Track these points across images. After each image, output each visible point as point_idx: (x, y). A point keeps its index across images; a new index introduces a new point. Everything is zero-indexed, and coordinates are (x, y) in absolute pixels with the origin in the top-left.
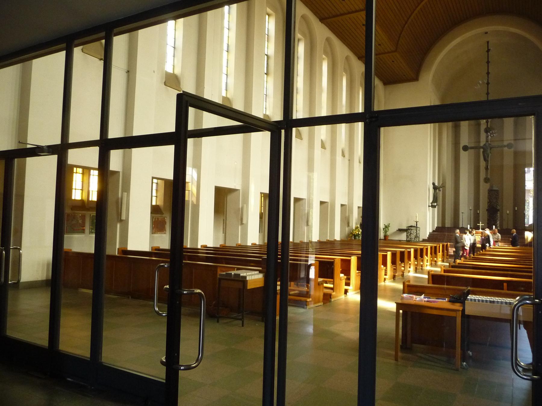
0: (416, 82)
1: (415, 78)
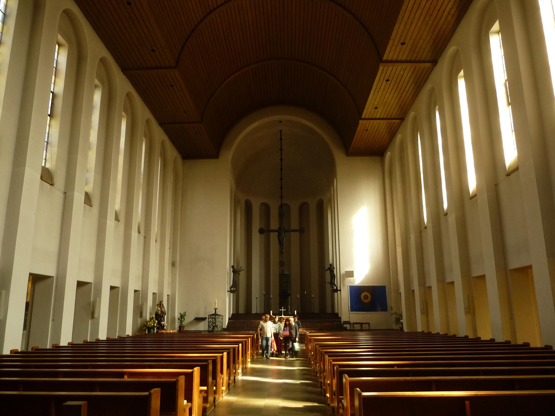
0: (214, 160)
1: (215, 155)
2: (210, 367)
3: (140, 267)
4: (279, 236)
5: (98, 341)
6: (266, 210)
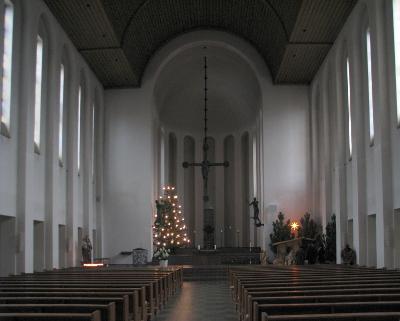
1: (138, 85)
2: (127, 301)
3: (64, 201)
4: (203, 169)
5: (24, 274)
6: (190, 143)
